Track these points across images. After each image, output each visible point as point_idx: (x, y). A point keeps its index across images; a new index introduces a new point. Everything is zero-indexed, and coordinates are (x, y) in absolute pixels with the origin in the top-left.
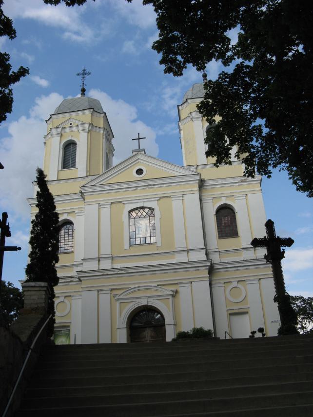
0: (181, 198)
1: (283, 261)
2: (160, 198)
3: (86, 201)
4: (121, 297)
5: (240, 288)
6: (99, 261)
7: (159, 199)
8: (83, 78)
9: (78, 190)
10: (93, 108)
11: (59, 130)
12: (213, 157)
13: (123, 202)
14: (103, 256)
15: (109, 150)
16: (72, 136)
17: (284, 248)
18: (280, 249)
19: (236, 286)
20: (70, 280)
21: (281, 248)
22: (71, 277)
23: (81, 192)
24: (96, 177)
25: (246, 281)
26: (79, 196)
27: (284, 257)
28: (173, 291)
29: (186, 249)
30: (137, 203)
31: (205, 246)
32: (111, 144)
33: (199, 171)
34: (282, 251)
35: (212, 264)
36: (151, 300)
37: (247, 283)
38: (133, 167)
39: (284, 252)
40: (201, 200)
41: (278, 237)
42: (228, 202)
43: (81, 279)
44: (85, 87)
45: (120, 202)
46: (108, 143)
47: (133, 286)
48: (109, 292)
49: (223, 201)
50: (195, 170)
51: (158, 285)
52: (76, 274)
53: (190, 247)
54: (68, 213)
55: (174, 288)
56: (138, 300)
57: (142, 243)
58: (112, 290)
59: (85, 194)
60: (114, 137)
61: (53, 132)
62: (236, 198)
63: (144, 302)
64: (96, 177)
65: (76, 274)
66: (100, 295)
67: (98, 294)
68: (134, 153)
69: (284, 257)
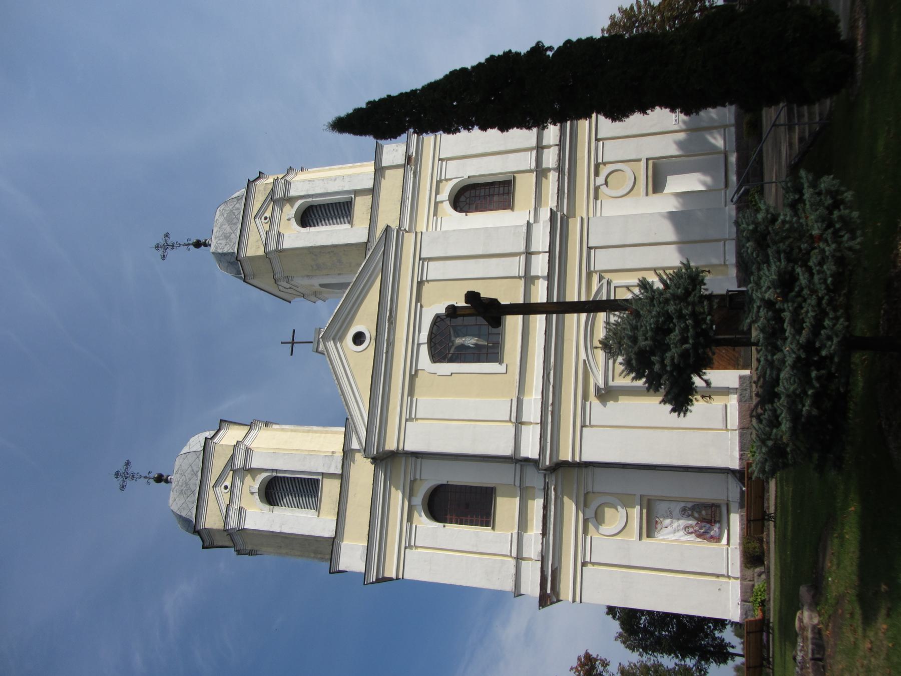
7: (419, 304)
20: (553, 493)
29: (523, 257)
49: (445, 195)
58: (585, 397)
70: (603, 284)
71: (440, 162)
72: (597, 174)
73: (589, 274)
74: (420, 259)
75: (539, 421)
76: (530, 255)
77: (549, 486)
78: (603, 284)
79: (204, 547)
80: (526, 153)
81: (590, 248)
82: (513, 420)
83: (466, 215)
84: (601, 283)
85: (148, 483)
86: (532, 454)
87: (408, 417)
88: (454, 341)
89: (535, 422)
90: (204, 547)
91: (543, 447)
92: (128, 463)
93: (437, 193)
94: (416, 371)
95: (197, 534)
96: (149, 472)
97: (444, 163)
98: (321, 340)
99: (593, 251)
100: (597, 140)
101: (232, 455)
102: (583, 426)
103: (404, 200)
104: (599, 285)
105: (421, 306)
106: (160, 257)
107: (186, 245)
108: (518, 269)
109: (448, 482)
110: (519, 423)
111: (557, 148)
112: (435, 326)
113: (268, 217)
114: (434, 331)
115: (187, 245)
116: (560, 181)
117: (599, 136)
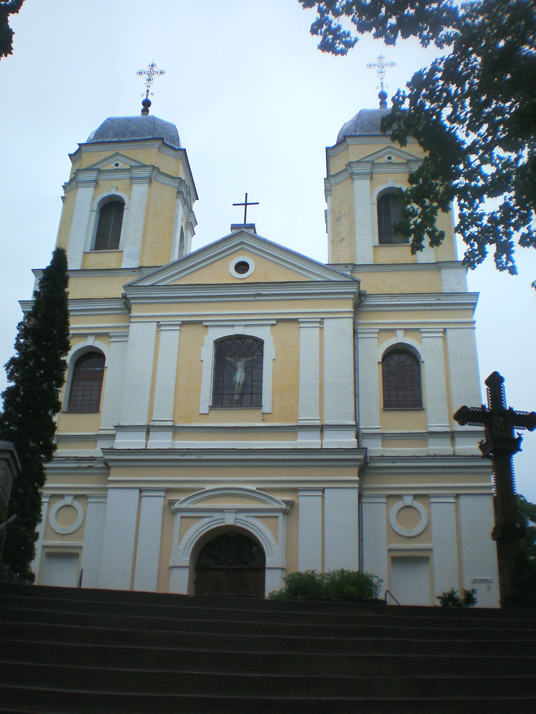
0: (318, 325)
1: (517, 459)
2: (278, 321)
3: (133, 314)
4: (185, 505)
5: (76, 510)
6: (148, 432)
7: (274, 322)
8: (149, 80)
9: (119, 292)
10: (163, 139)
11: (92, 176)
12: (339, 55)
13: (205, 324)
14: (157, 424)
15: (187, 223)
16: (117, 189)
17: (520, 431)
18: (512, 433)
19: (69, 503)
20: (87, 465)
21: (516, 431)
22: (91, 459)
23: (124, 297)
24: (156, 270)
25: (111, 337)
26: (119, 305)
27: (520, 450)
28: (285, 502)
29: (318, 423)
30: (233, 326)
31: (355, 420)
32: (191, 211)
33: (357, 276)
34: (516, 436)
35: (366, 457)
36: (242, 516)
37: (433, 500)
38: (231, 257)
39: (520, 439)
40: (355, 332)
41: (511, 409)
42: (409, 340)
43: (110, 464)
44: (150, 98)
45: (200, 323)
46: (186, 207)
47: (208, 487)
48: (163, 494)
49: (400, 338)
50: (349, 273)
51: (257, 489)
52: (101, 455)
53: (327, 422)
54: (97, 336)
55: (288, 498)
56: (217, 516)
57: (221, 396)
58: (168, 491)
59: (132, 301)
60: (198, 199)
61: (83, 177)
62: (424, 335)
63: (229, 520)
64: (156, 270)
65: (101, 455)
66: (364, 506)
67: (140, 498)
68: (235, 231)
69: (520, 450)
70: (282, 504)
71: (443, 330)
72: (415, 497)
73: (295, 490)
74: (322, 319)
75: (148, 448)
76: (320, 430)
77: (93, 462)
78: (282, 504)
79: (327, 149)
80: (353, 417)
81: (323, 490)
82: (152, 423)
83: (379, 363)
84: (282, 503)
85: (377, 88)
86: (118, 443)
87: (161, 323)
88: (241, 361)
89: (148, 444)
90: (327, 149)
91: (120, 452)
92: (392, 64)
93: (406, 330)
94: (207, 326)
95: (343, 139)
96: (152, 94)
97: (441, 335)
98: (240, 230)
99: (320, 493)
100: (457, 496)
101: (146, 165)
102: (141, 490)
103: (398, 297)
104: (280, 501)
105: (273, 325)
106: (140, 69)
107: (382, 84)
108: (307, 418)
109: (107, 367)
110: (148, 429)
111: (452, 453)
112: (252, 341)
113: (391, 160)
114: (247, 340)
115: (382, 85)
116: (444, 458)
117: (326, 491)
